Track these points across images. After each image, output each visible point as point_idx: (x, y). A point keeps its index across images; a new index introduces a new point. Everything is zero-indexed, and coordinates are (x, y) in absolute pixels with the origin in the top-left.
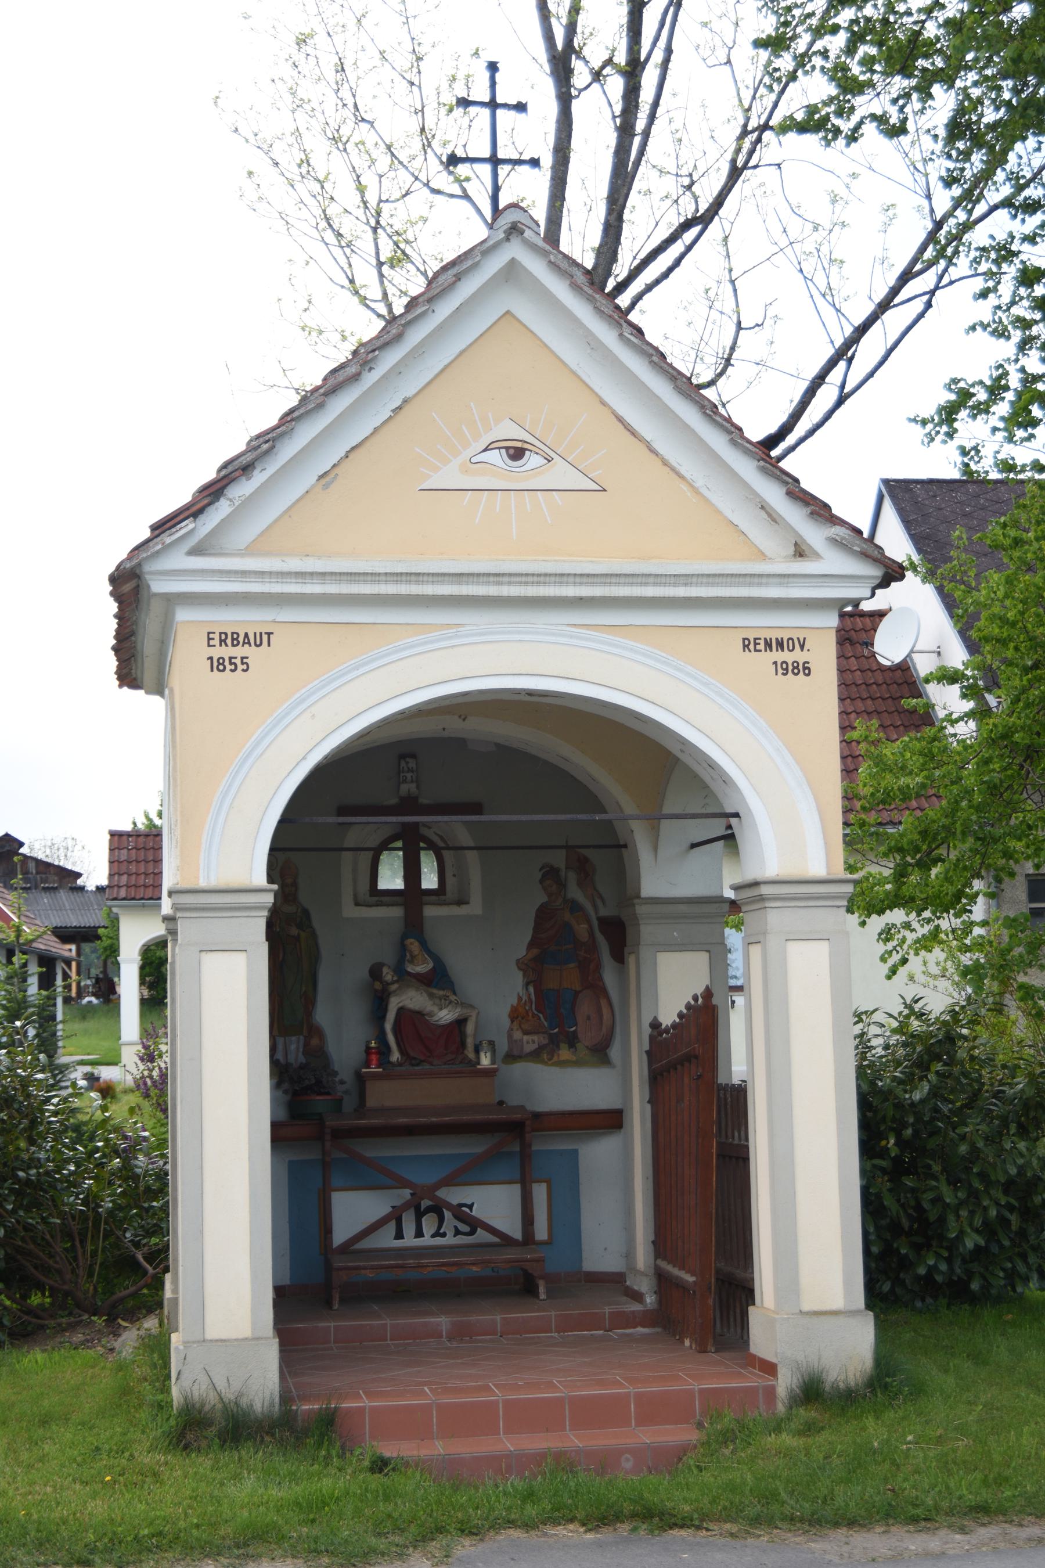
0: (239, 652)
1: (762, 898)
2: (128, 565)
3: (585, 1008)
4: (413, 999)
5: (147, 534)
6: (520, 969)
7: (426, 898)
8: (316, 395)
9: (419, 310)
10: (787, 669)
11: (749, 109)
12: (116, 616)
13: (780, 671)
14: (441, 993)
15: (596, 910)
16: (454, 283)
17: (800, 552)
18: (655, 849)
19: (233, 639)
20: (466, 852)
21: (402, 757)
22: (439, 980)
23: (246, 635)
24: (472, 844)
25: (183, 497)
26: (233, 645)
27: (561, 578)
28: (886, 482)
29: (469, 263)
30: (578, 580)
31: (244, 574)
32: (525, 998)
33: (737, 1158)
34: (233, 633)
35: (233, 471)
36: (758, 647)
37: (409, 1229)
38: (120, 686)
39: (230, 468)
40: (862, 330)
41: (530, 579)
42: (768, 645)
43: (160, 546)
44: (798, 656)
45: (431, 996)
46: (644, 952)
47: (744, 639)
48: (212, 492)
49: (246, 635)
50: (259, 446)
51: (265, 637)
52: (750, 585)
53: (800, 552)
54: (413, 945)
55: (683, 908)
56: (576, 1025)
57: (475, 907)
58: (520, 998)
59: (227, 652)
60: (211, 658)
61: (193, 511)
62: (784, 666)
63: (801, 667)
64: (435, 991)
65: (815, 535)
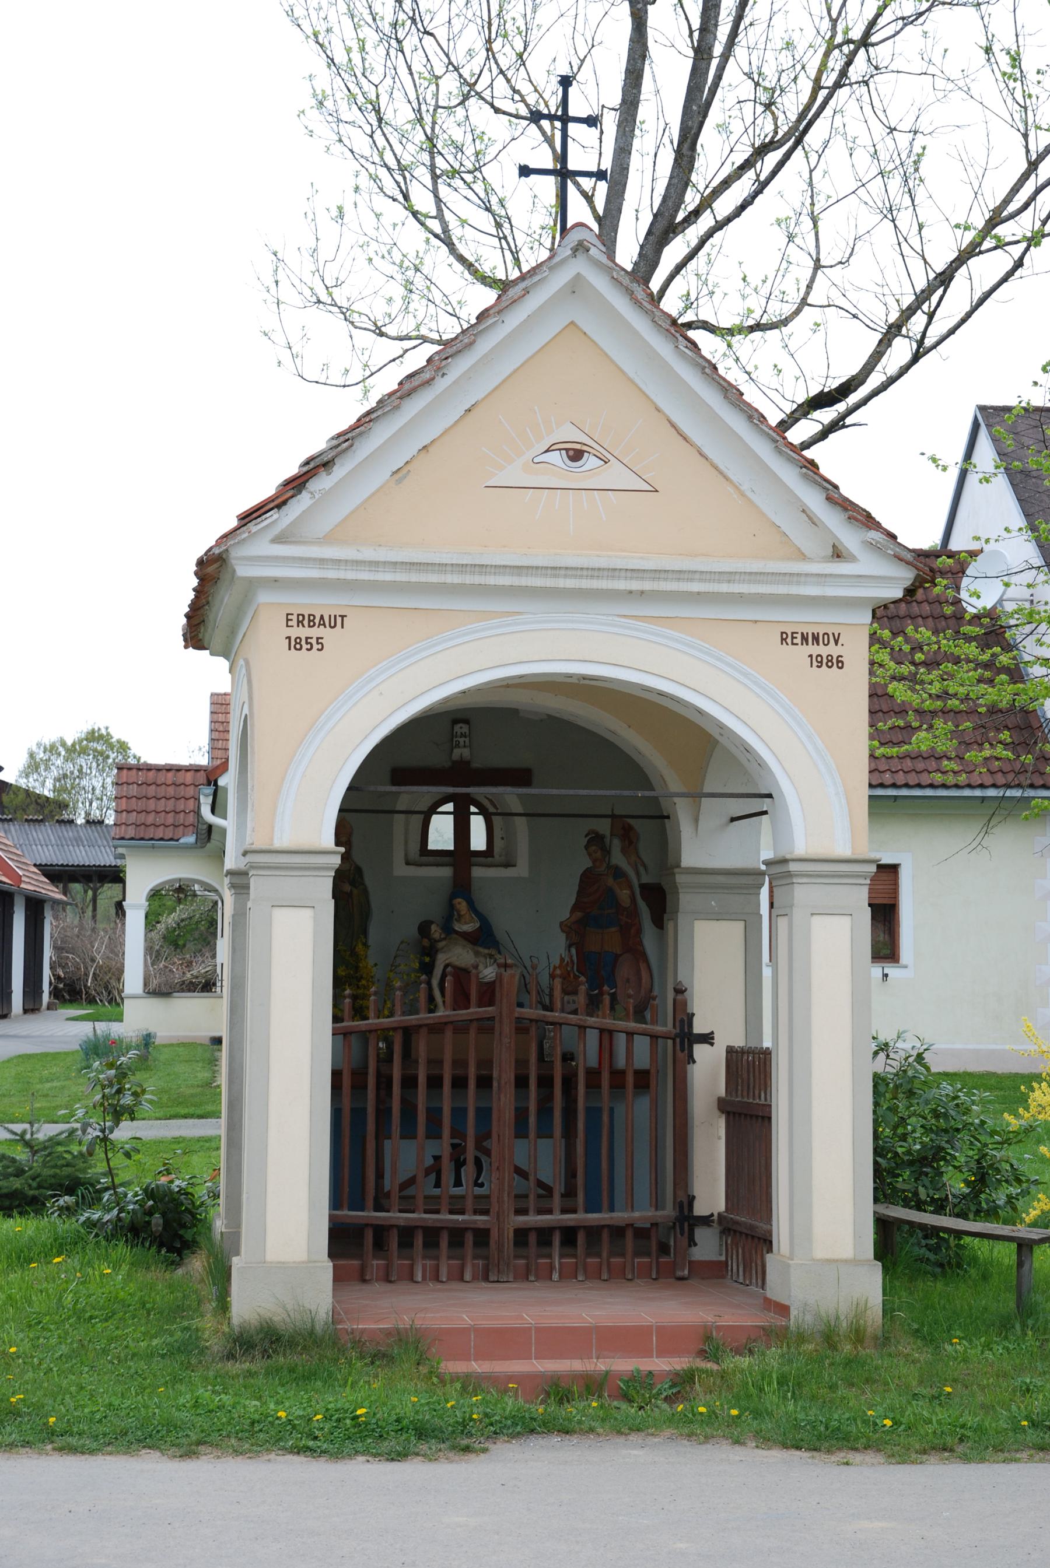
0: (315, 632)
1: (789, 874)
2: (217, 551)
3: (624, 971)
4: (461, 955)
5: (234, 523)
6: (563, 931)
7: (474, 860)
8: (393, 398)
9: (491, 321)
10: (821, 662)
11: (836, 20)
12: (194, 590)
13: (815, 664)
14: (486, 951)
15: (638, 874)
16: (524, 295)
17: (838, 554)
18: (696, 820)
19: (309, 621)
20: (516, 818)
21: (455, 722)
22: (484, 938)
23: (322, 617)
24: (521, 810)
25: (268, 490)
26: (309, 626)
27: (613, 572)
28: (982, 409)
29: (536, 278)
30: (629, 574)
31: (322, 562)
32: (567, 959)
33: (763, 1117)
34: (309, 615)
35: (316, 467)
36: (795, 641)
37: (448, 1176)
38: (186, 647)
39: (312, 465)
40: (945, 279)
41: (585, 573)
42: (805, 638)
43: (246, 535)
44: (833, 650)
45: (477, 954)
46: (682, 919)
47: (782, 633)
48: (295, 485)
49: (322, 617)
50: (339, 445)
51: (339, 620)
52: (790, 583)
53: (838, 554)
54: (462, 905)
55: (721, 879)
56: (616, 987)
57: (522, 869)
58: (562, 960)
59: (303, 632)
60: (289, 638)
61: (277, 502)
62: (819, 659)
63: (834, 661)
64: (481, 950)
65: (850, 538)
